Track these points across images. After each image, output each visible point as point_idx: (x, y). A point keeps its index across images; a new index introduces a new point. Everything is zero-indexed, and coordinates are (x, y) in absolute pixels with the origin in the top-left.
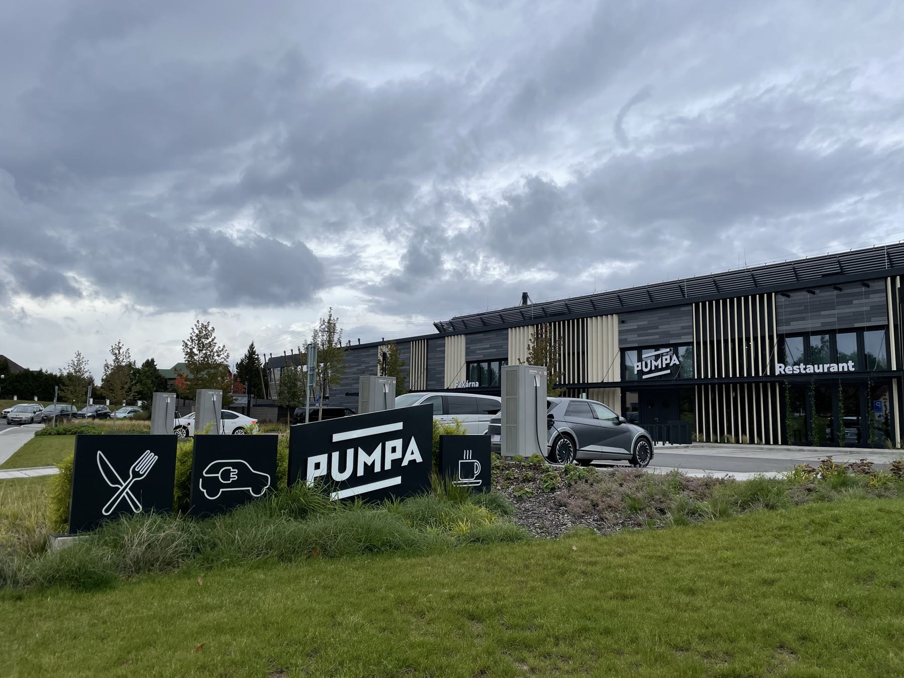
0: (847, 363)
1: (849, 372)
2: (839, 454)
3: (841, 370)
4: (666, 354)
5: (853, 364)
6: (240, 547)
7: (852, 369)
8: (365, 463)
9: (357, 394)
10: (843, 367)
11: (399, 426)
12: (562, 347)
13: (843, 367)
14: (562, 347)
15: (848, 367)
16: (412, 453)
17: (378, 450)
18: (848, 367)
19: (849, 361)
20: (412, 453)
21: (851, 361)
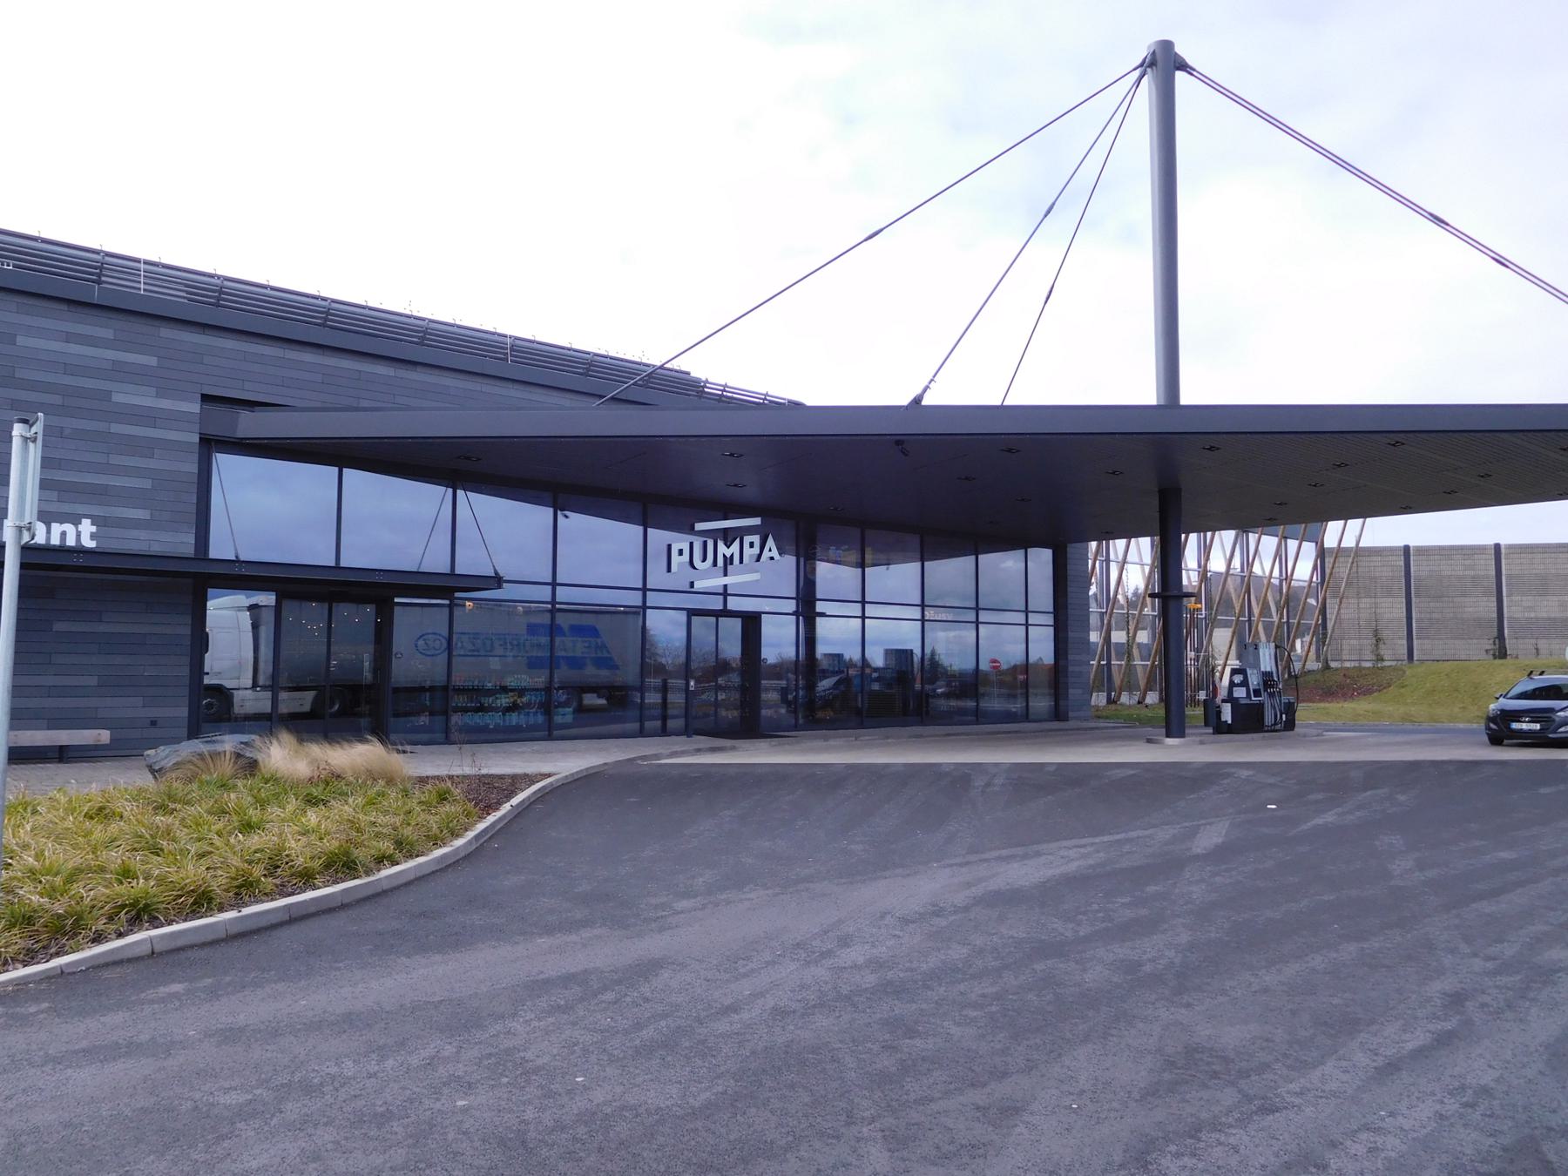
0: (76, 522)
1: (80, 551)
2: (1431, 218)
3: (55, 541)
4: (1535, 551)
5: (94, 529)
6: (330, 1001)
7: (89, 543)
8: (724, 555)
9: (1497, 547)
10: (64, 534)
11: (756, 521)
12: (116, 428)
13: (64, 534)
14: (116, 428)
15: (78, 535)
16: (770, 550)
17: (736, 544)
18: (78, 535)
19: (84, 521)
20: (770, 550)
21: (89, 521)
